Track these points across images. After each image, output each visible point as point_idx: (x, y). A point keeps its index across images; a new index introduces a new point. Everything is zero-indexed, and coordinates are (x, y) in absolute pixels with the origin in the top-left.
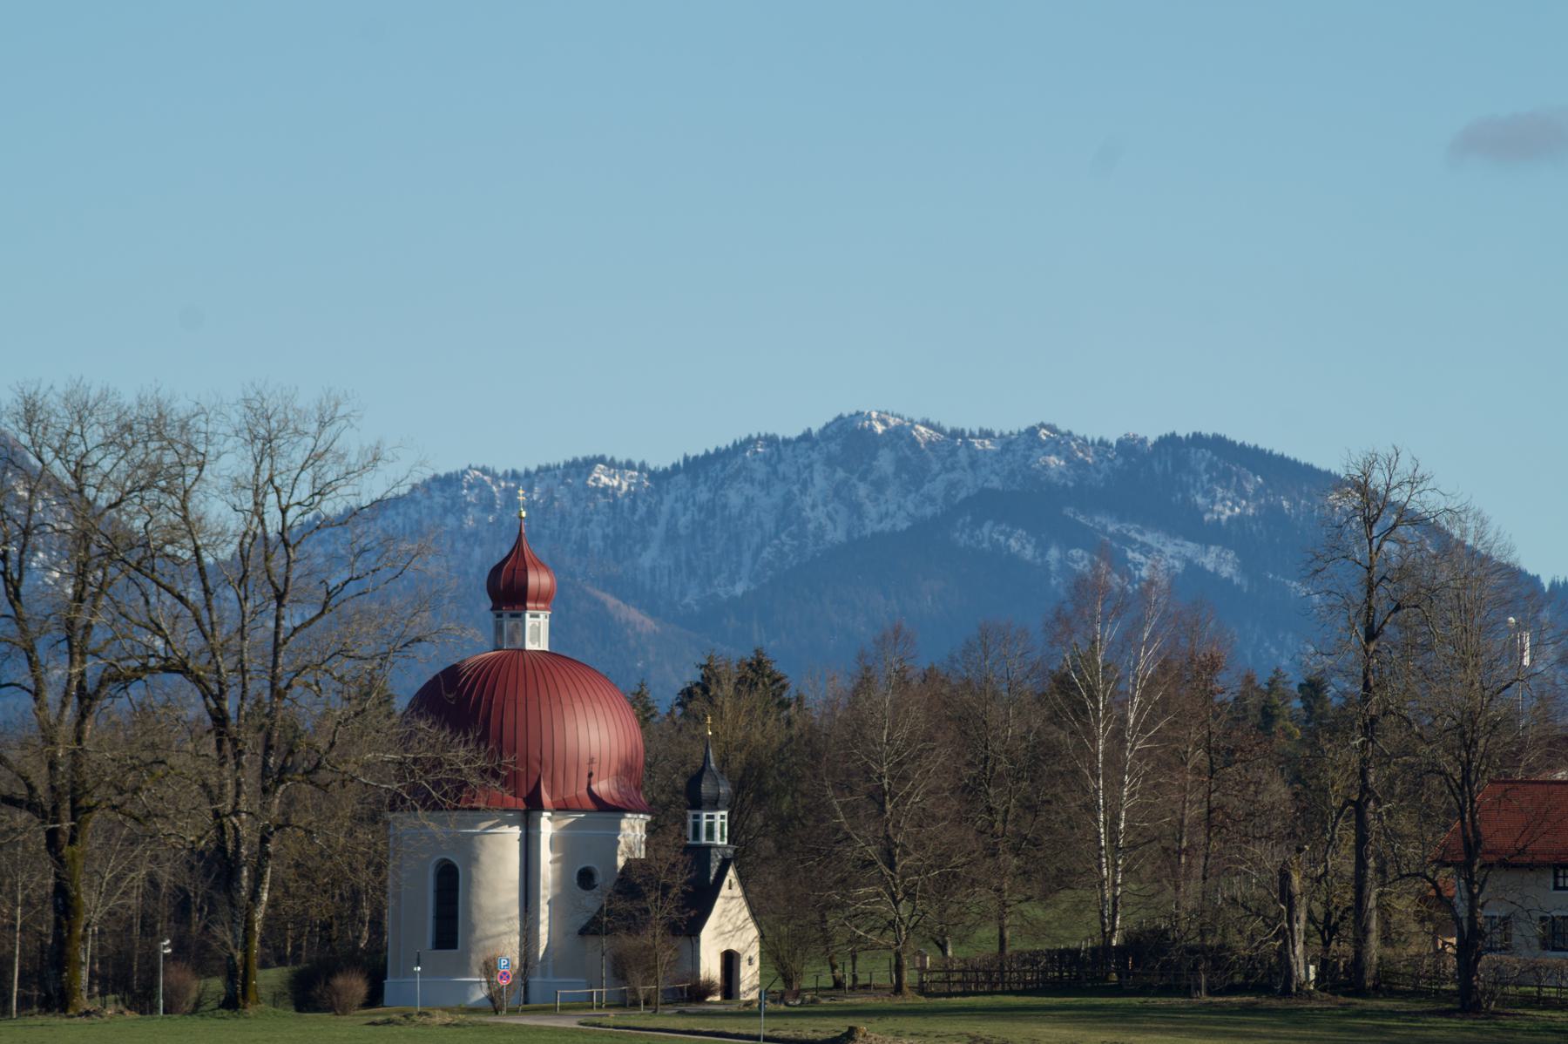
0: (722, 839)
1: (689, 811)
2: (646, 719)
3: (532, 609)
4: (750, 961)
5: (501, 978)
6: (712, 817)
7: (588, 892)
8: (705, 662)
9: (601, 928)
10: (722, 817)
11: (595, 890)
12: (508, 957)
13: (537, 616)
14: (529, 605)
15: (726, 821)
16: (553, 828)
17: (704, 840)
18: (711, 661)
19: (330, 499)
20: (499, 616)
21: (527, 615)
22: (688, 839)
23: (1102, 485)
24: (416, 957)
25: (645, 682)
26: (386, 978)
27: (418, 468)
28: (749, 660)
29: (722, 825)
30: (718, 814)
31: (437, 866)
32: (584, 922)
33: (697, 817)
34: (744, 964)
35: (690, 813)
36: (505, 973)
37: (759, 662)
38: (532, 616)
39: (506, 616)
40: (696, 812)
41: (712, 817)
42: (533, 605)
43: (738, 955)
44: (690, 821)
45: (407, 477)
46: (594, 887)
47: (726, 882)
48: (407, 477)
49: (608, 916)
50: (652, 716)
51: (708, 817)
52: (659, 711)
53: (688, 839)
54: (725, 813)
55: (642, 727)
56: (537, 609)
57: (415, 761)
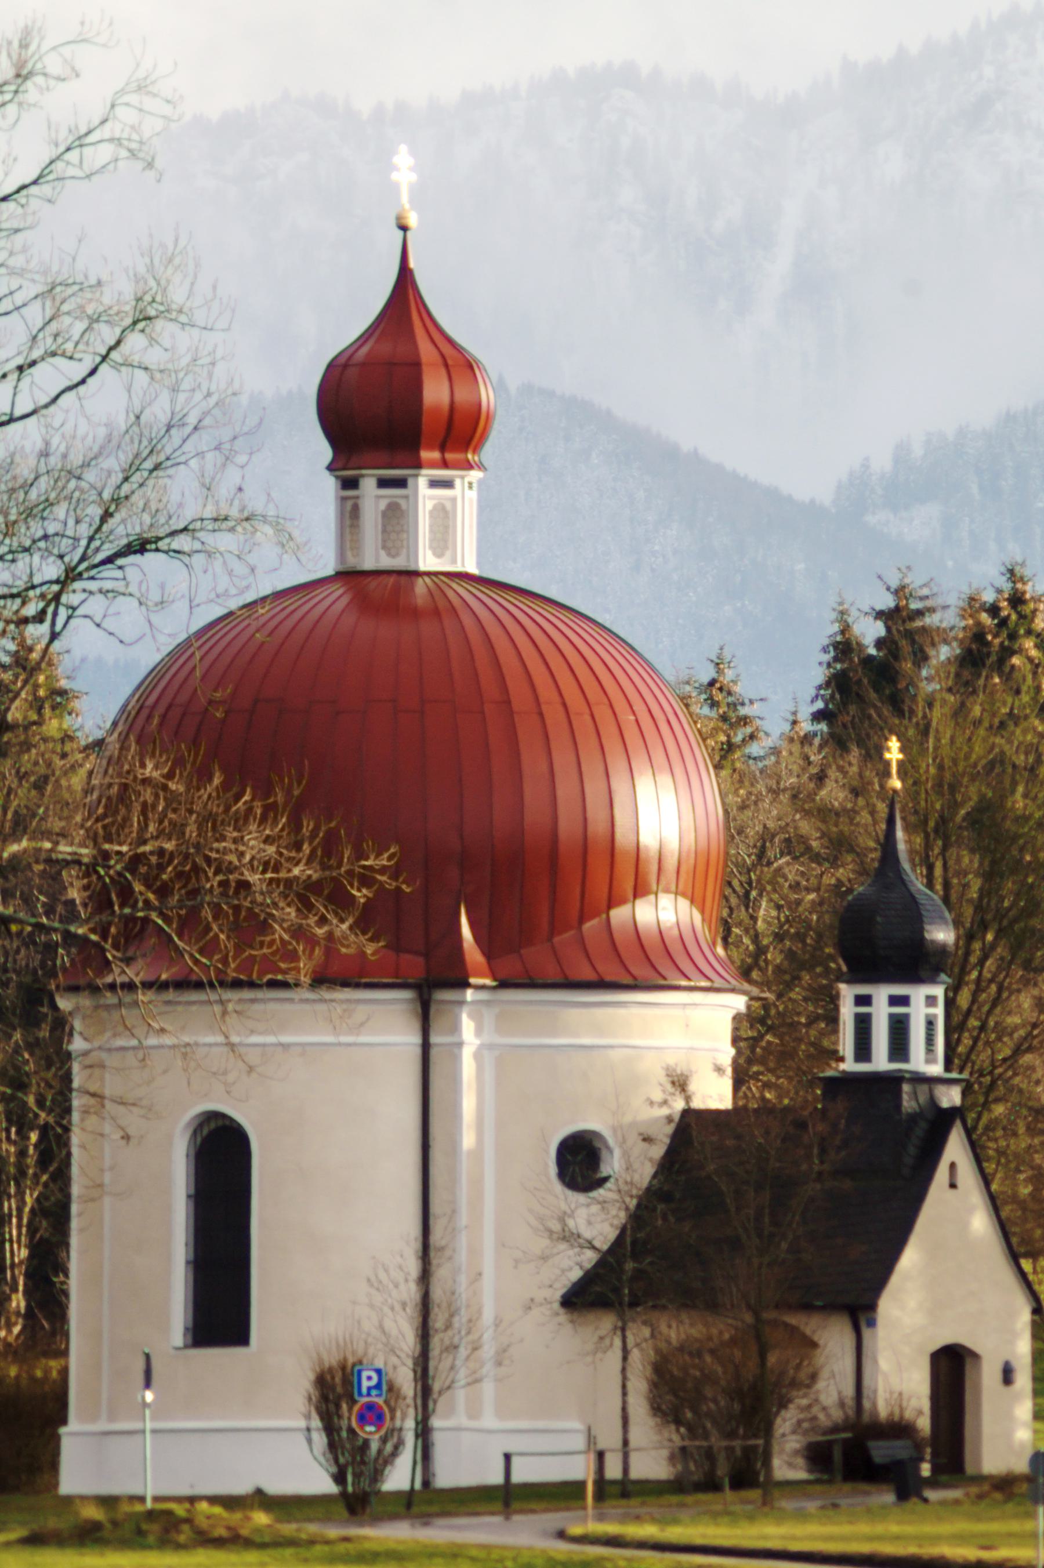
0: (930, 1059)
1: (843, 987)
2: (729, 748)
3: (433, 465)
4: (1008, 1375)
5: (362, 1420)
6: (904, 1001)
7: (581, 1198)
8: (888, 602)
9: (617, 1290)
10: (931, 1001)
11: (600, 1193)
12: (379, 1364)
13: (448, 484)
14: (425, 455)
15: (939, 1011)
16: (668, 925)
17: (881, 1061)
18: (720, 671)
19: (48, 182)
20: (350, 484)
21: (422, 482)
22: (842, 1059)
23: (737, 1406)
24: (140, 1365)
25: (727, 655)
26: (64, 1421)
27: (133, 98)
28: (989, 597)
29: (930, 1023)
30: (918, 993)
31: (200, 1127)
32: (576, 1274)
33: (863, 1000)
34: (989, 1374)
35: (847, 992)
36: (370, 1407)
37: (1017, 600)
38: (434, 484)
39: (368, 484)
40: (863, 990)
41: (904, 1001)
42: (436, 455)
43: (975, 1356)
44: (847, 1011)
45: (104, 122)
46: (606, 1179)
47: (942, 1174)
48: (104, 122)
49: (635, 1256)
50: (752, 737)
51: (894, 1000)
52: (765, 725)
53: (842, 1059)
54: (938, 991)
55: (718, 767)
56: (445, 464)
57: (136, 861)
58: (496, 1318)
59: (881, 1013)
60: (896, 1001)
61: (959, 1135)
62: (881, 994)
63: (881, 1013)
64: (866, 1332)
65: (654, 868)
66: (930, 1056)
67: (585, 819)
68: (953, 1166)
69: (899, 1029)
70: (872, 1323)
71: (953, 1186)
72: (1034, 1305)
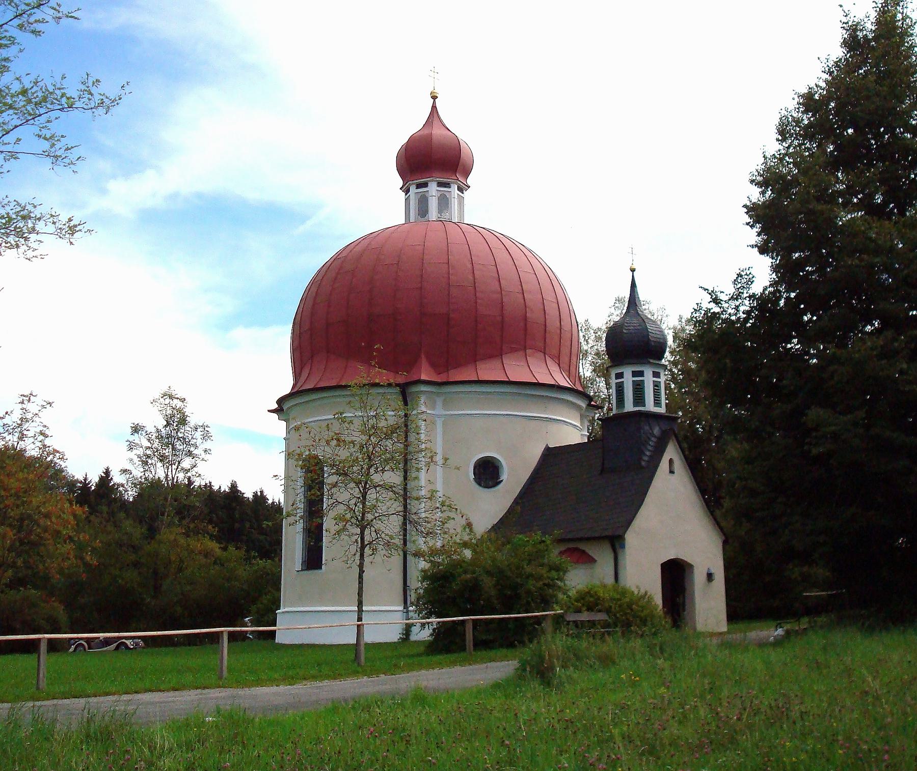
17: (629, 407)
34: (699, 577)
41: (641, 374)
46: (502, 481)
47: (664, 464)
58: (599, 612)
59: (628, 381)
60: (635, 374)
61: (675, 445)
62: (628, 371)
63: (628, 381)
64: (620, 551)
65: (556, 338)
66: (620, 387)
67: (545, 325)
68: (671, 461)
69: (639, 389)
70: (623, 546)
71: (672, 472)
72: (723, 538)
